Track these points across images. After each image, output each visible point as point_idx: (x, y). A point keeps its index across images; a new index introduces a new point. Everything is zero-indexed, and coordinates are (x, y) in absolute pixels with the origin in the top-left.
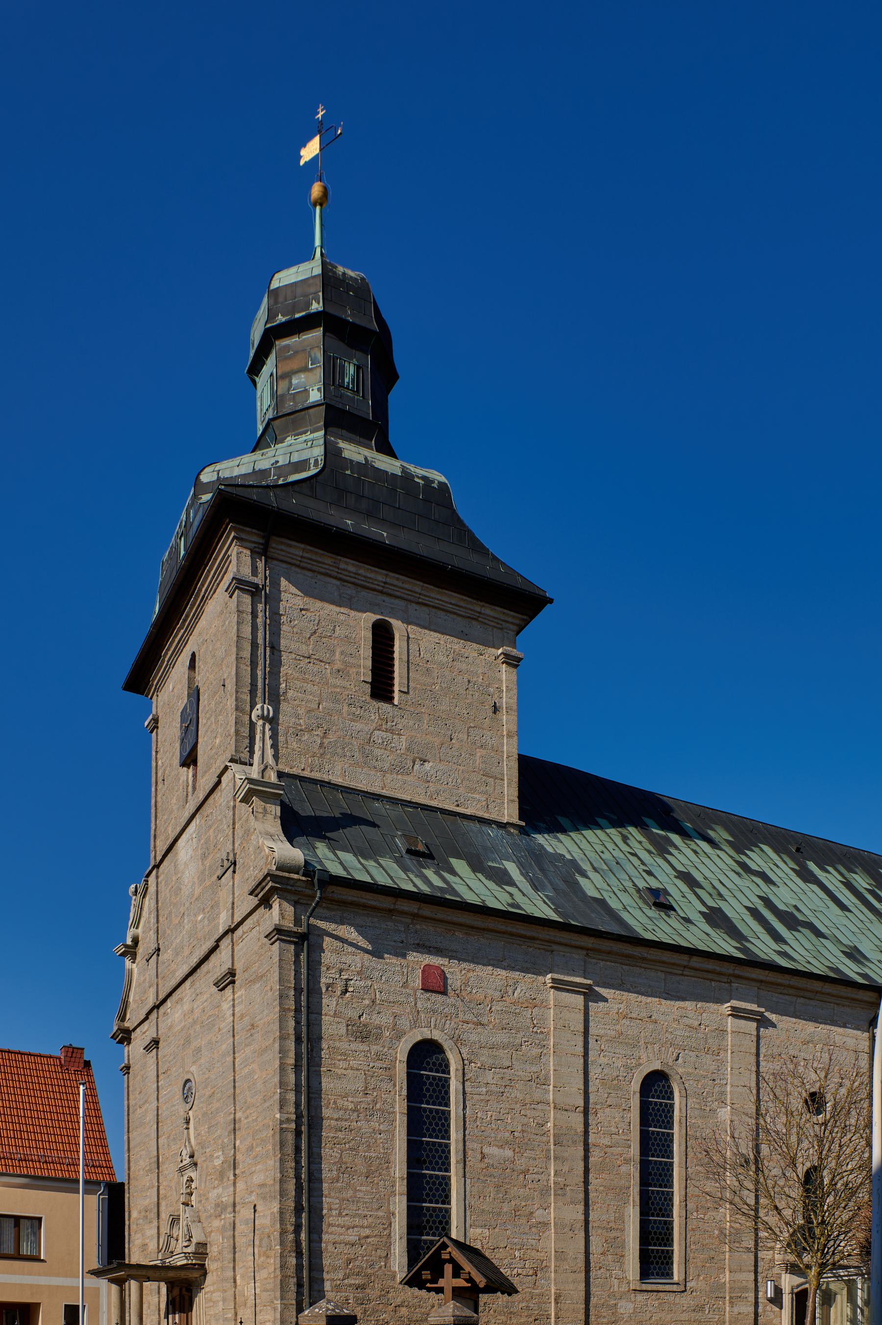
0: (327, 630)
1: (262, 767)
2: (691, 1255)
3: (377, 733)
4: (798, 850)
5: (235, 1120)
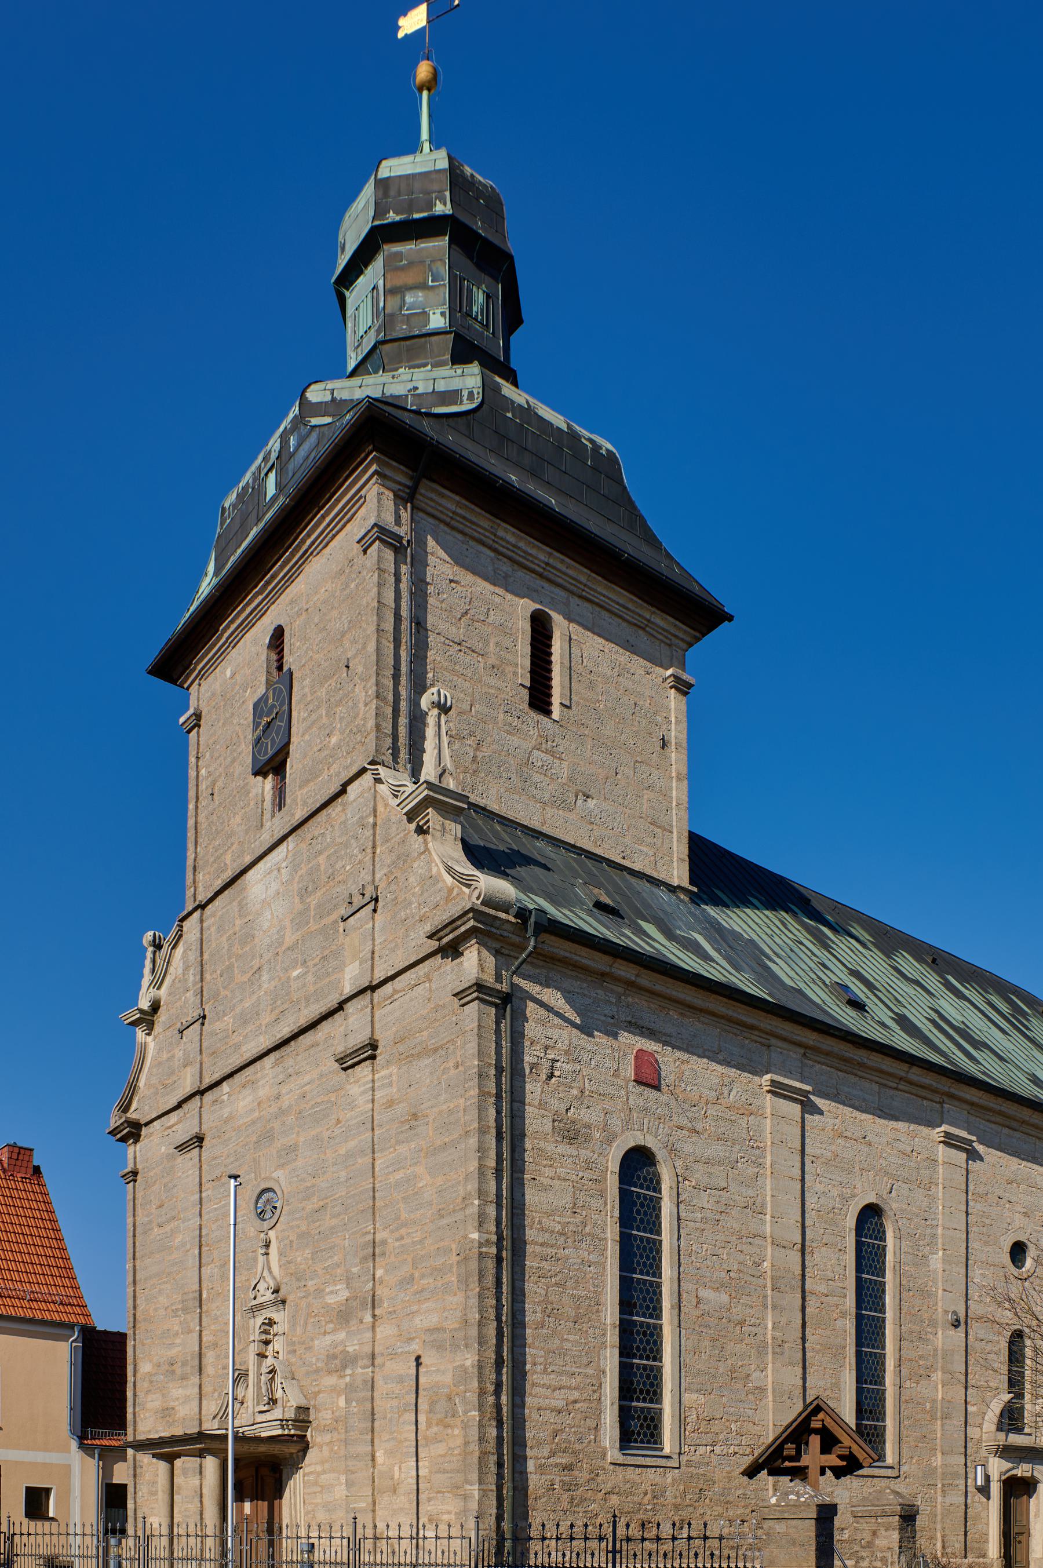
0: (481, 613)
2: (904, 1433)
3: (536, 753)
4: (934, 961)
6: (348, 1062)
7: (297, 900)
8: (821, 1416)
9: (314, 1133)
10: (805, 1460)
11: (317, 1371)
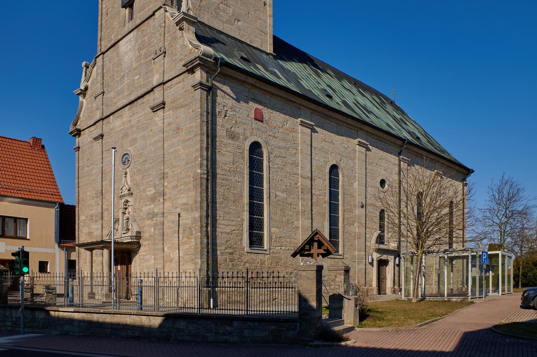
2: (345, 243)
3: (221, 5)
4: (355, 83)
6: (155, 109)
7: (137, 52)
8: (318, 236)
9: (143, 134)
10: (312, 251)
11: (144, 219)
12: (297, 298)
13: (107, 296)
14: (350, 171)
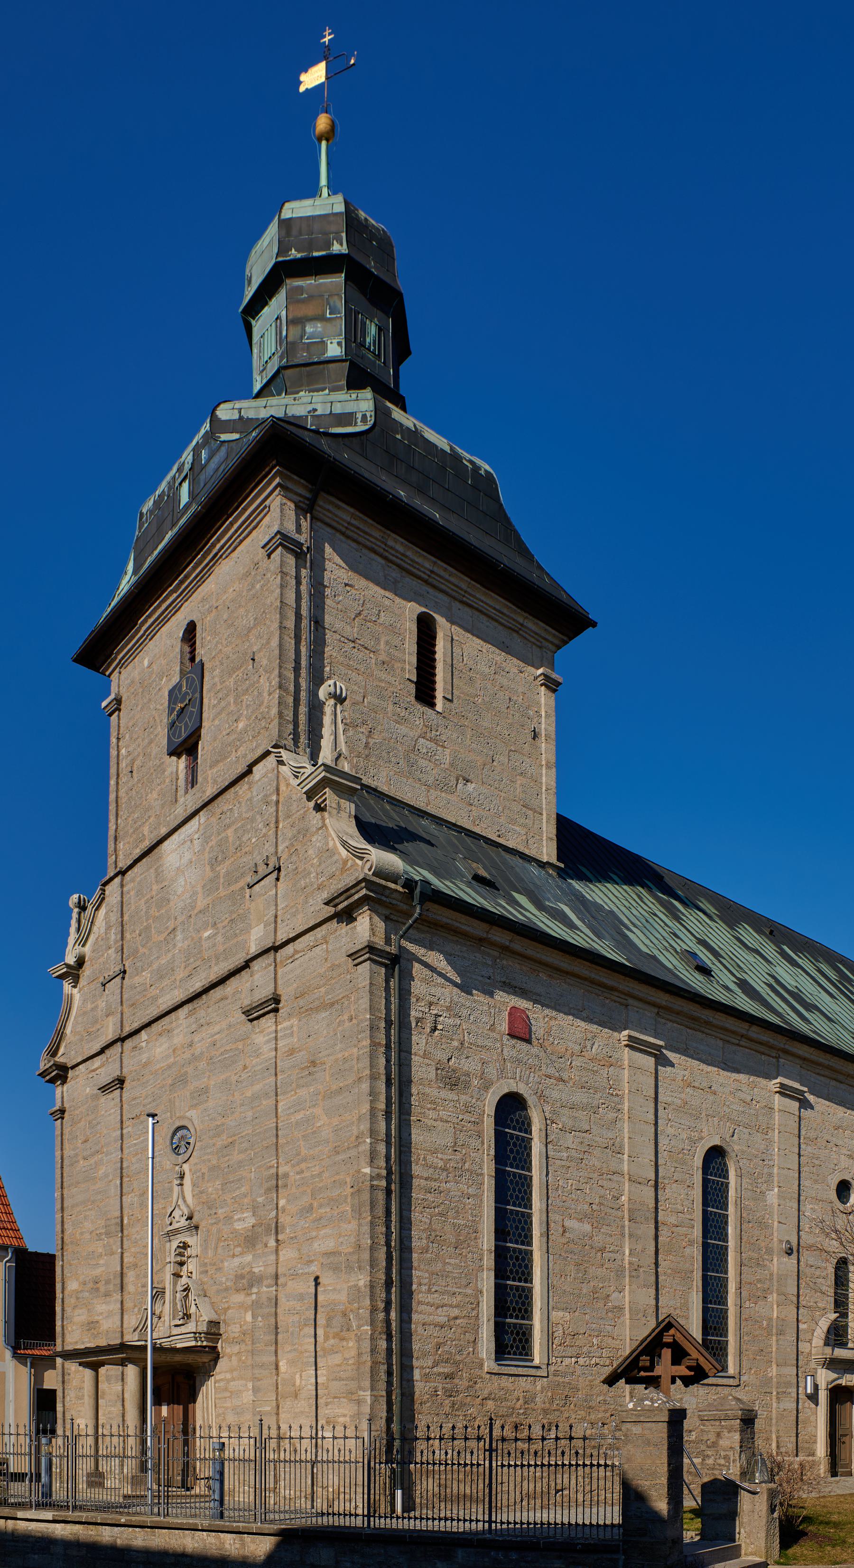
0: (371, 614)
1: (336, 755)
2: (744, 1347)
3: (421, 741)
4: (771, 932)
5: (277, 1175)
7: (208, 868)
9: (223, 1077)
10: (658, 1371)
11: (227, 1289)
12: (617, 1488)
13: (136, 1481)
14: (757, 1161)
